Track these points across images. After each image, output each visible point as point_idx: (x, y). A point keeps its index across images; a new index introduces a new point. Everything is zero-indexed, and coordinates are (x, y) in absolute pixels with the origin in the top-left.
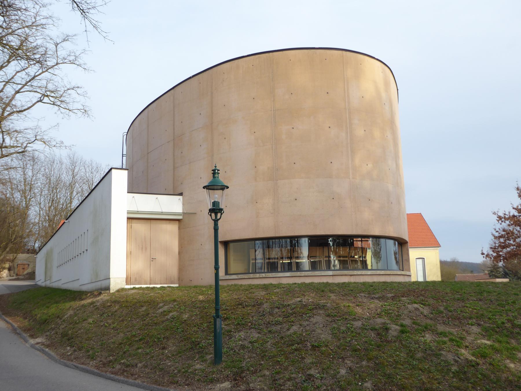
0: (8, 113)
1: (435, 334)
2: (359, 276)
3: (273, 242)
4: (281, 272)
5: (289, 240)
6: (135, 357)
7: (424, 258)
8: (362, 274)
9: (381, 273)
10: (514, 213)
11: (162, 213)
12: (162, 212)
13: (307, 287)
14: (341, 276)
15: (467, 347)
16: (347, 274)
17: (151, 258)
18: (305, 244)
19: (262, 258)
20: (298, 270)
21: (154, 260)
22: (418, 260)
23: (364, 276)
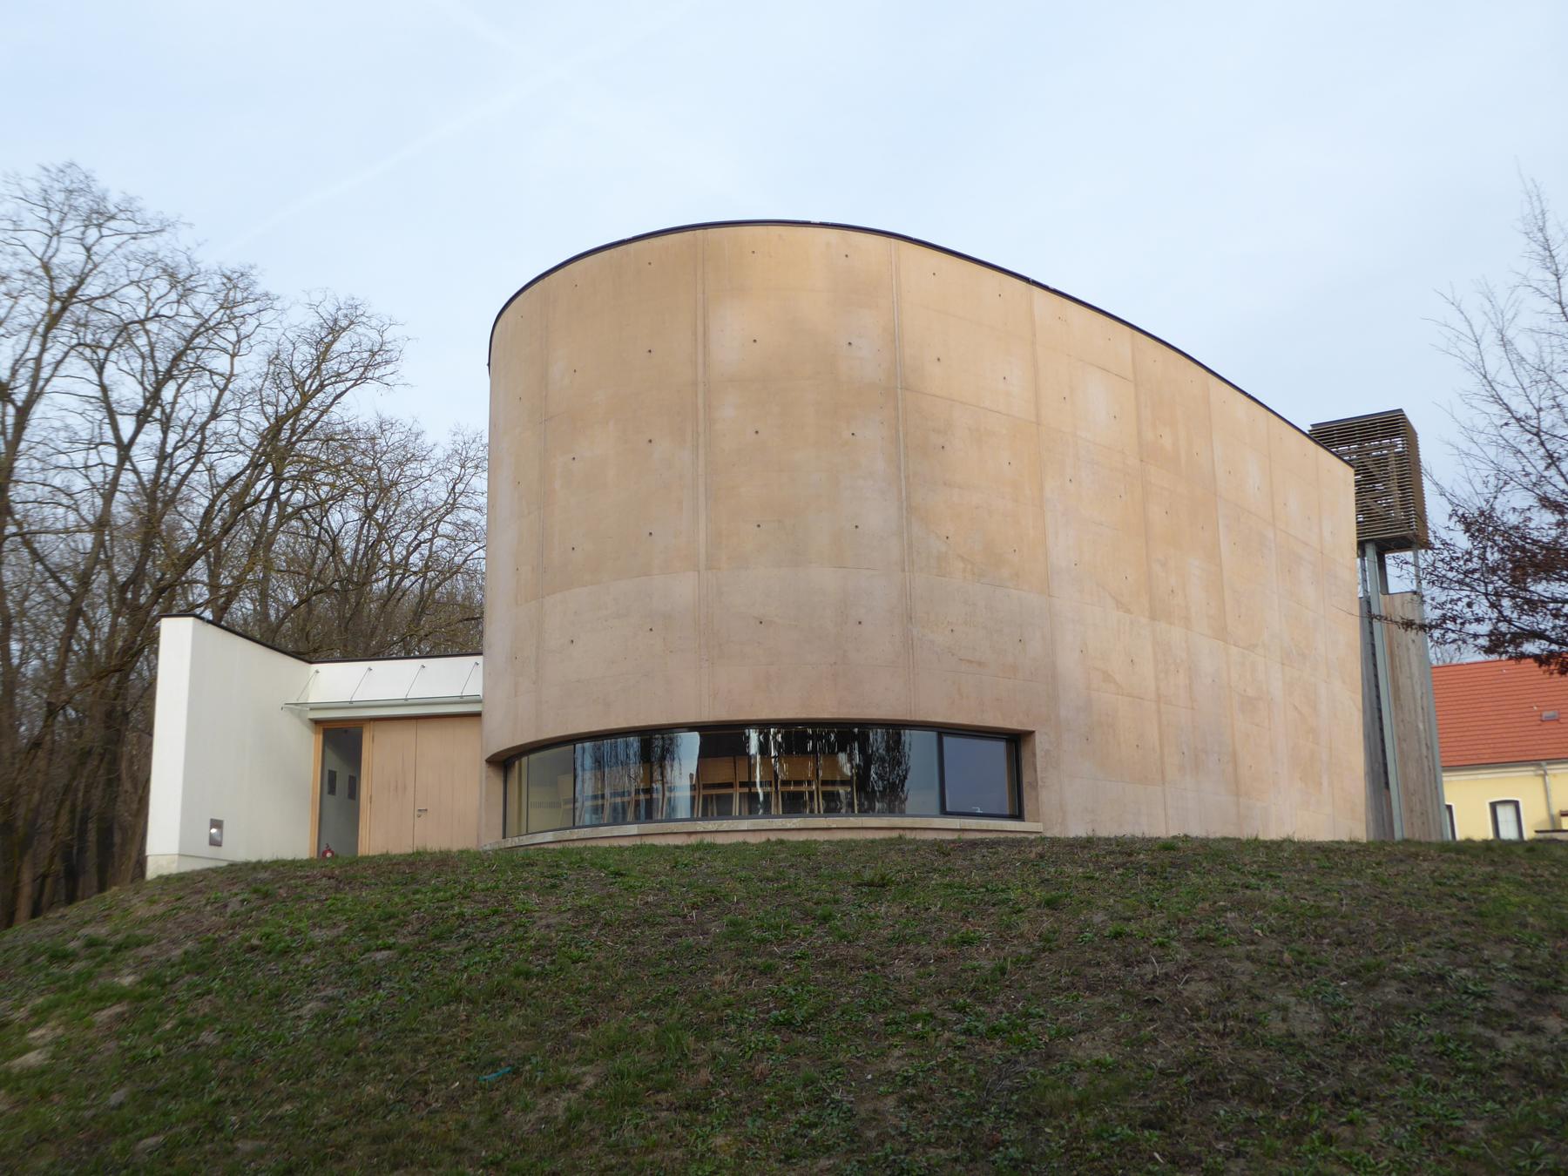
1: (1329, 944)
3: (583, 749)
4: (741, 817)
5: (634, 742)
9: (789, 826)
11: (406, 703)
13: (437, 890)
15: (1196, 1015)
17: (416, 809)
18: (690, 744)
20: (651, 818)
21: (423, 814)
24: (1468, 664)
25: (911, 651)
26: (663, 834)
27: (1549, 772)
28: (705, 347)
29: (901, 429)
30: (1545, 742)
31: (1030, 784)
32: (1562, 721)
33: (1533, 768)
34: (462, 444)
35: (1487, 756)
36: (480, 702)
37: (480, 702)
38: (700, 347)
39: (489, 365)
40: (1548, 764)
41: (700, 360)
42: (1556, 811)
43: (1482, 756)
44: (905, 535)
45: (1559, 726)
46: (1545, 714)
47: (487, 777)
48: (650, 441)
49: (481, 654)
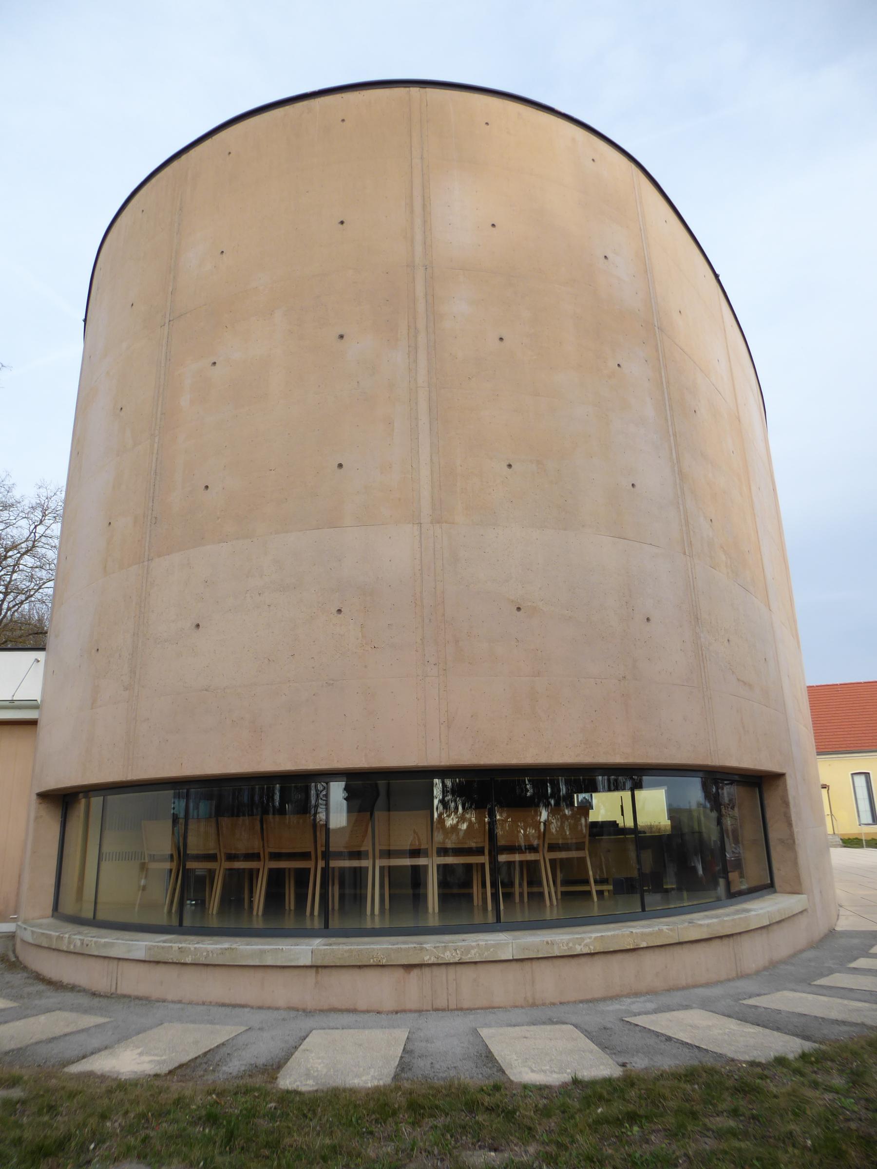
0: (31, 536)
2: (451, 970)
6: (713, 798)
7: (869, 773)
8: (466, 959)
10: (225, 861)
12: (12, 701)
14: (356, 972)
16: (384, 962)
18: (337, 791)
19: (172, 856)
22: (856, 778)
23: (482, 970)
26: (360, 967)
28: (425, 222)
29: (663, 374)
31: (782, 841)
34: (44, 498)
36: (37, 707)
37: (37, 707)
38: (418, 221)
39: (85, 320)
41: (419, 237)
44: (681, 508)
47: (36, 818)
48: (341, 337)
49: (43, 649)
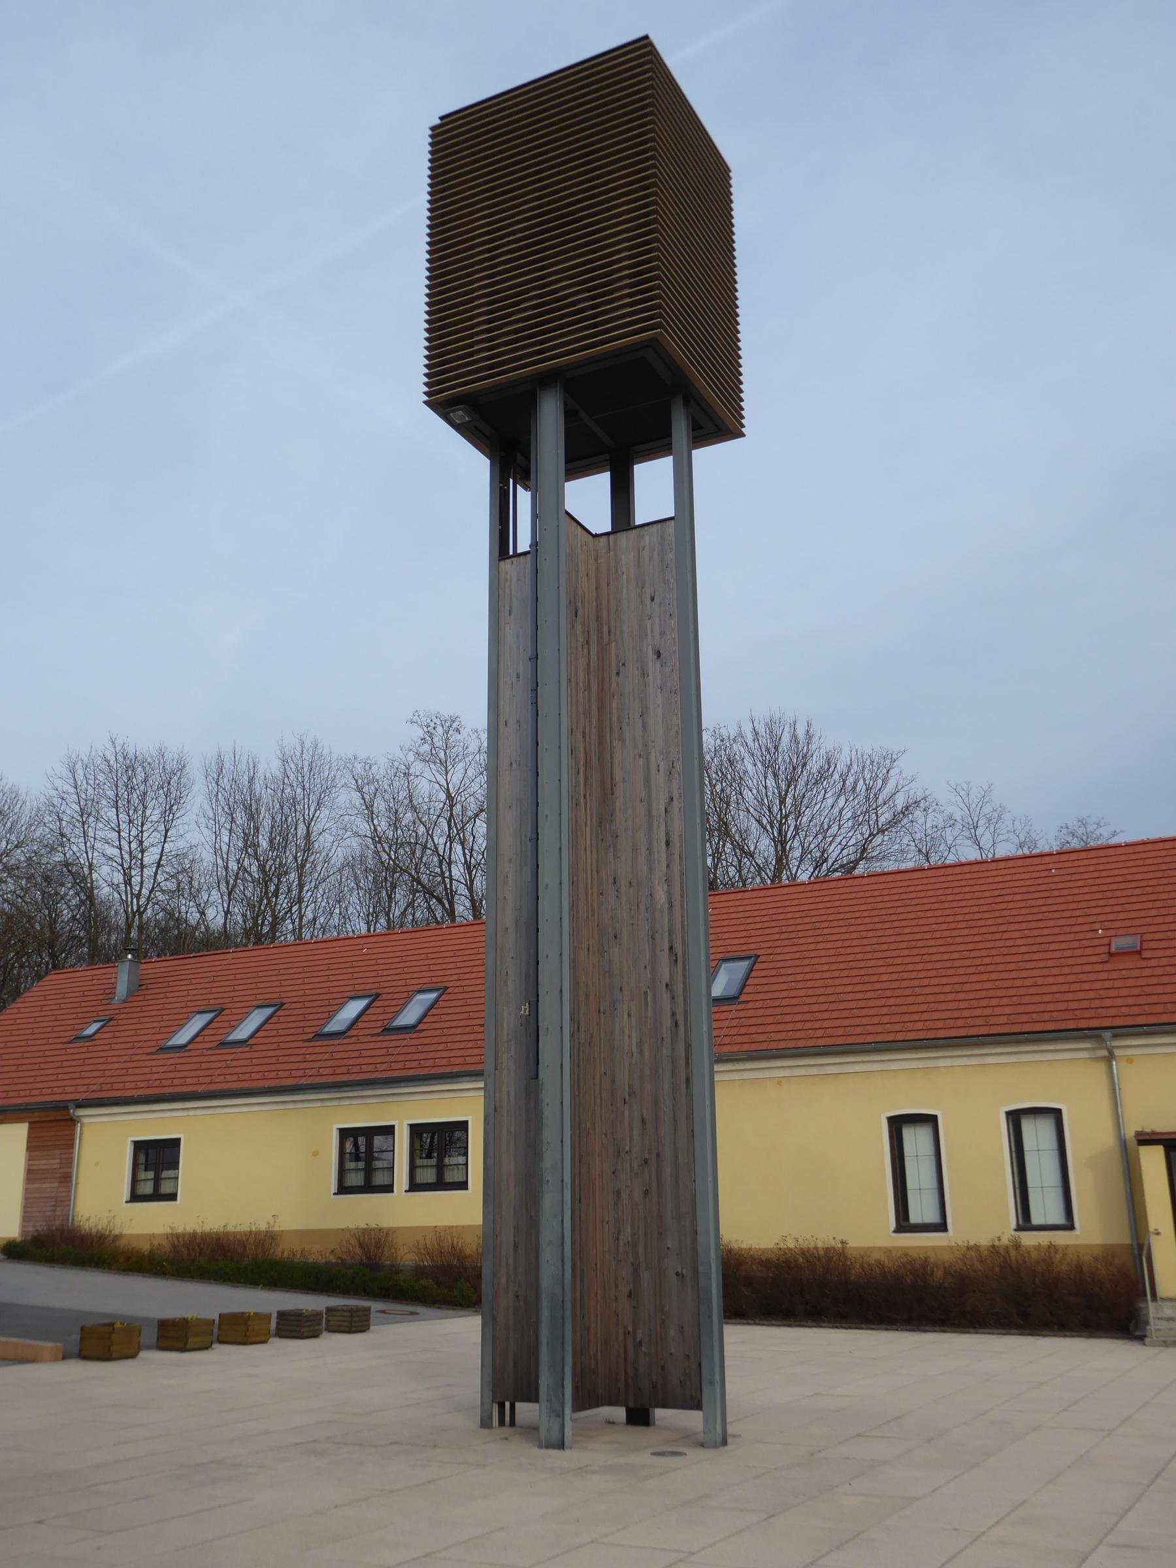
24: (1127, 845)
25: (574, 728)
27: (1117, 1052)
30: (1051, 980)
32: (1145, 954)
33: (1087, 1045)
35: (1003, 1020)
40: (1115, 1036)
42: (1130, 1133)
43: (993, 1020)
45: (1143, 964)
46: (1117, 944)
